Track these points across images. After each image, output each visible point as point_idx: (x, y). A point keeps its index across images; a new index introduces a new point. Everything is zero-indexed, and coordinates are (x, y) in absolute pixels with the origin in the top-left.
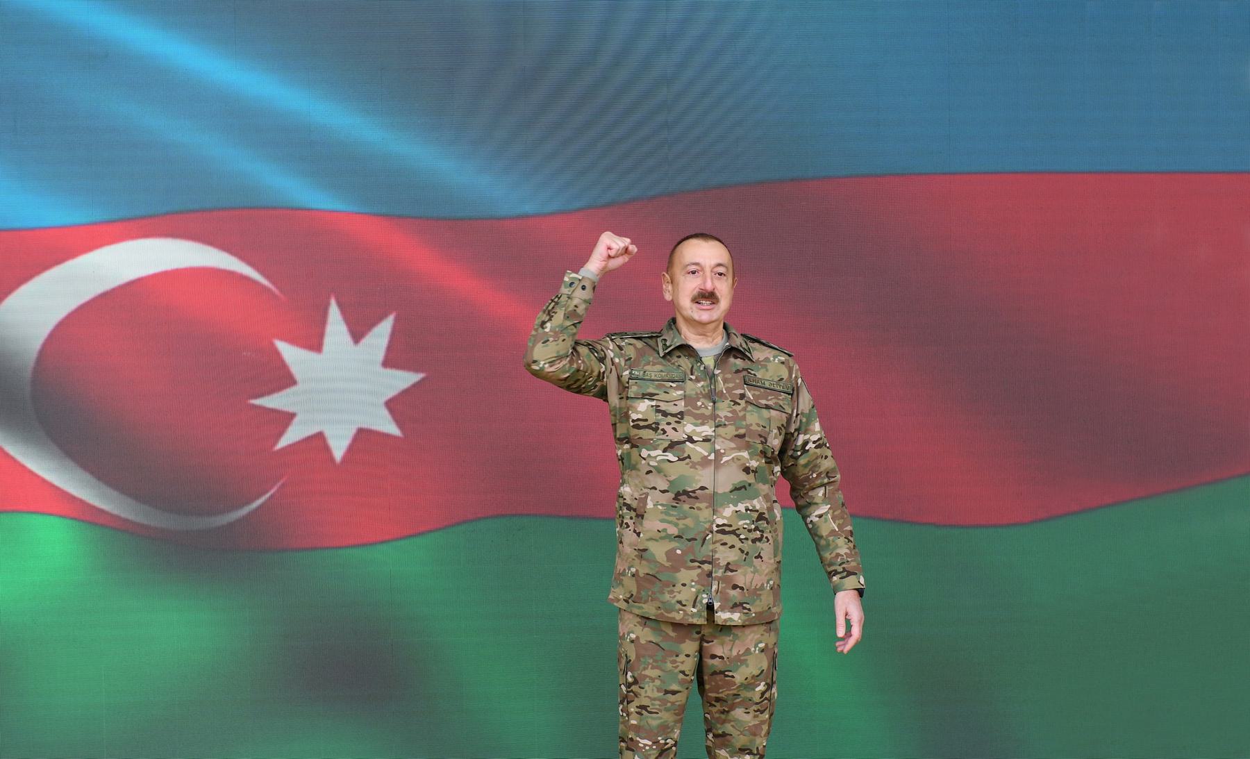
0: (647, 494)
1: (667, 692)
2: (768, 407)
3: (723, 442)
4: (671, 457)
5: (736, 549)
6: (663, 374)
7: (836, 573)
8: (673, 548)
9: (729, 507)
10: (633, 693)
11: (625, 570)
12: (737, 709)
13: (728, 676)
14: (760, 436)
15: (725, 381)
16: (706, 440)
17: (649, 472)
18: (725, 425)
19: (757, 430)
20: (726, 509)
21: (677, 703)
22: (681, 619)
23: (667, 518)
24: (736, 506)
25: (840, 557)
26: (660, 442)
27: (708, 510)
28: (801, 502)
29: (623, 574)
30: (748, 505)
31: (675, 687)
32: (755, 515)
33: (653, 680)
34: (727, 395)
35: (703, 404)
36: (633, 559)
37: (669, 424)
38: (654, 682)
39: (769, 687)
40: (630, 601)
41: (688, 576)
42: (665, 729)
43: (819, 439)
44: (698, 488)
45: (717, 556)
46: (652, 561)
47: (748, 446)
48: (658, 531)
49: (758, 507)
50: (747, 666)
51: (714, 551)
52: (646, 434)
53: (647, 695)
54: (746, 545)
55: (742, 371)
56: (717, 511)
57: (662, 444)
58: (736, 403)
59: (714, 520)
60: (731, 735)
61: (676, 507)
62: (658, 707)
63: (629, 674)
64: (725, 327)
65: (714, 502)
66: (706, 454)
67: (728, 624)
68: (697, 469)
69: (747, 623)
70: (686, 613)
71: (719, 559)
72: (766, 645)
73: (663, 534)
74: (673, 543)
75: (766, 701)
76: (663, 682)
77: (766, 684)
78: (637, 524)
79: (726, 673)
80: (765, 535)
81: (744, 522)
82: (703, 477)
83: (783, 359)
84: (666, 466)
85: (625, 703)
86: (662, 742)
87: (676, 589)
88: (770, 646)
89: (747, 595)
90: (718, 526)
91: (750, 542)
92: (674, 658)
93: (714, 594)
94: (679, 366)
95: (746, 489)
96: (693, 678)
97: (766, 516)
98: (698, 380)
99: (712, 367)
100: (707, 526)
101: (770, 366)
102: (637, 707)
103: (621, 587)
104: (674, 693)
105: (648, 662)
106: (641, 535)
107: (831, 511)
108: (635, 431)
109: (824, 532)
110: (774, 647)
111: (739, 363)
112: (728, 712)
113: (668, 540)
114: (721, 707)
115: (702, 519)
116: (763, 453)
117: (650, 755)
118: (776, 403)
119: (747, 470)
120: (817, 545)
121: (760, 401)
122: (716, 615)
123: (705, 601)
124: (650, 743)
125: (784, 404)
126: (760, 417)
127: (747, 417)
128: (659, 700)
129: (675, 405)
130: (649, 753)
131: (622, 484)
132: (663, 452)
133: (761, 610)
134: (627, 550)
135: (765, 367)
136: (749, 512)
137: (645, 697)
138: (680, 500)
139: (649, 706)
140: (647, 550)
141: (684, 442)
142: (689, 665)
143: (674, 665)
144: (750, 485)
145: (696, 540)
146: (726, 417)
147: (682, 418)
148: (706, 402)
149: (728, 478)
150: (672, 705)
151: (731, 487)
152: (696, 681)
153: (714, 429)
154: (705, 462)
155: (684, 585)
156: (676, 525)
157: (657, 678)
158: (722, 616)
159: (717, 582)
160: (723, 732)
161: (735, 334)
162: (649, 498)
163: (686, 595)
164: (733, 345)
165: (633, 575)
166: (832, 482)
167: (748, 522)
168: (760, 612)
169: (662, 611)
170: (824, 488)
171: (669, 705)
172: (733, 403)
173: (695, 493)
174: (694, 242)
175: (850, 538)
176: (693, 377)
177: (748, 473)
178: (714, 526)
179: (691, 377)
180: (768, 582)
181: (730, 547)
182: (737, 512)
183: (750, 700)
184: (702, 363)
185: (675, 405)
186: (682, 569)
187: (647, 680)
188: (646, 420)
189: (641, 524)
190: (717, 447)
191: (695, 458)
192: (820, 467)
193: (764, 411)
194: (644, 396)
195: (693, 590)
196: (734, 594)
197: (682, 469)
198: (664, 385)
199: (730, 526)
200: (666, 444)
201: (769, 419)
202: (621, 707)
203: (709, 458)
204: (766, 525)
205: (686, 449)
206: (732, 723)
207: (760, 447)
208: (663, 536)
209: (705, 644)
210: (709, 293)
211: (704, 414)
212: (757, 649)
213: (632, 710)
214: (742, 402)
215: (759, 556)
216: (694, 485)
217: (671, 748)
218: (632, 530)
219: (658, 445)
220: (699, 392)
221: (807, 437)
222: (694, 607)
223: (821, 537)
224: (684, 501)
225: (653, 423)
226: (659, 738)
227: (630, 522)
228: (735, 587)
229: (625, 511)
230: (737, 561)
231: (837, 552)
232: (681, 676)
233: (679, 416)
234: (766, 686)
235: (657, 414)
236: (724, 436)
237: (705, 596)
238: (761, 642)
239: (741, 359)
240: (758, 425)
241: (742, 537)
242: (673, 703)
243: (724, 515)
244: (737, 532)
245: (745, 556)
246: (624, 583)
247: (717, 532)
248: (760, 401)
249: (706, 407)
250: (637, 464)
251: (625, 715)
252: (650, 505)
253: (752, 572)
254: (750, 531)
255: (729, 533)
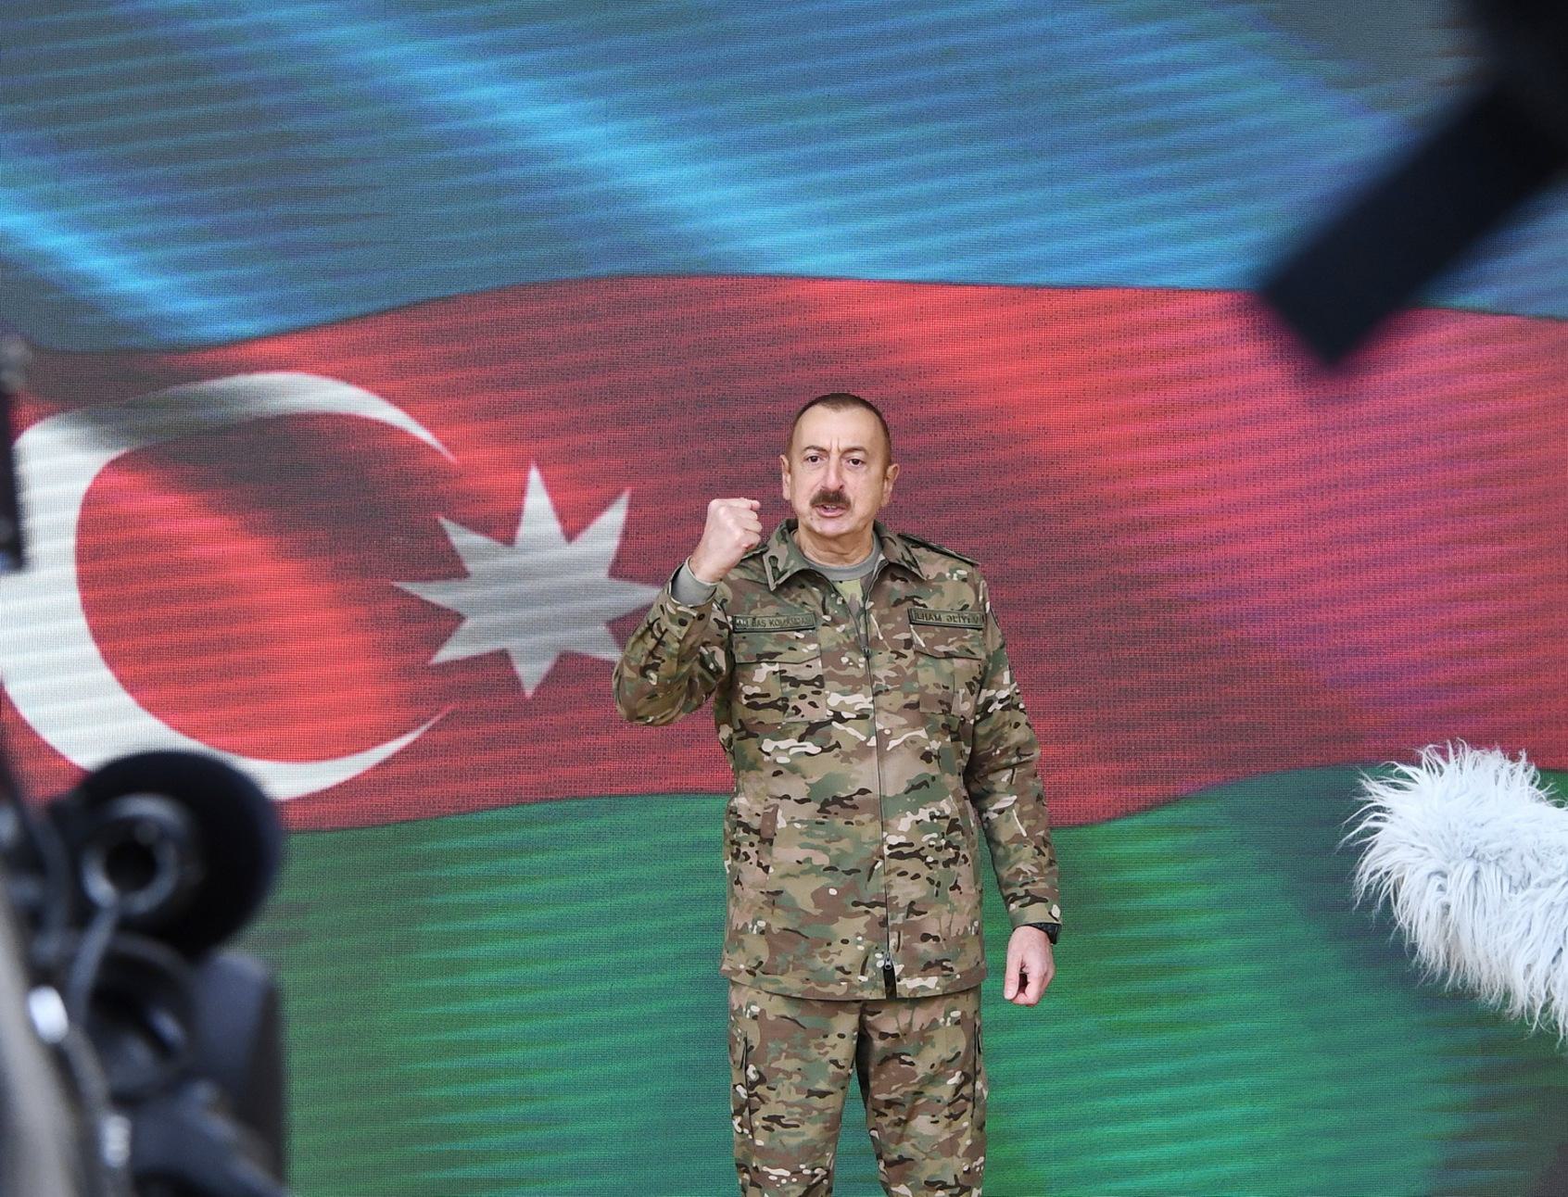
0: (776, 808)
1: (811, 1093)
2: (949, 656)
3: (886, 717)
4: (810, 747)
5: (923, 878)
6: (782, 619)
7: (1015, 898)
8: (823, 887)
9: (906, 816)
10: (759, 1097)
11: (746, 924)
12: (919, 1116)
13: (904, 1062)
14: (941, 702)
15: (881, 621)
16: (862, 716)
17: (777, 774)
18: (887, 690)
19: (937, 695)
20: (903, 820)
21: (829, 1112)
22: (845, 994)
23: (810, 841)
24: (915, 813)
25: (1022, 875)
26: (793, 726)
27: (873, 824)
28: (974, 788)
29: (744, 929)
30: (933, 809)
31: (822, 1086)
32: (945, 824)
33: (789, 1075)
34: (885, 643)
35: (850, 660)
36: (761, 908)
37: (803, 697)
38: (791, 1078)
39: (968, 1078)
40: (757, 971)
41: (853, 927)
42: (810, 1152)
43: (1008, 697)
44: (856, 791)
45: (893, 893)
46: (792, 908)
47: (924, 721)
48: (798, 862)
49: (948, 812)
50: (933, 1046)
51: (888, 886)
52: (769, 716)
53: (780, 1099)
54: (935, 872)
55: (904, 601)
56: (888, 825)
57: (795, 729)
58: (901, 656)
59: (884, 840)
60: (912, 1160)
61: (822, 823)
62: (797, 1116)
63: (752, 1068)
64: (876, 529)
65: (882, 810)
66: (863, 738)
67: (918, 996)
68: (851, 763)
69: (950, 990)
70: (851, 985)
71: (897, 897)
72: (963, 1013)
73: (806, 866)
74: (822, 878)
75: (962, 1101)
76: (805, 1077)
77: (963, 1073)
78: (763, 854)
79: (903, 1057)
80: (962, 853)
81: (929, 836)
82: (863, 775)
83: (963, 573)
84: (804, 762)
85: (746, 1113)
86: (807, 1172)
87: (831, 949)
88: (970, 1015)
89: (945, 948)
90: (890, 847)
91: (941, 867)
92: (822, 1040)
93: (892, 951)
94: (804, 603)
95: (928, 786)
96: (850, 1071)
97: (959, 823)
98: (835, 622)
99: (859, 598)
100: (874, 848)
101: (946, 587)
102: (764, 1119)
103: (740, 951)
104: (822, 1094)
105: (781, 1049)
106: (771, 870)
107: (1017, 805)
108: (754, 713)
109: (1004, 836)
110: (974, 1017)
111: (898, 586)
112: (906, 1122)
113: (814, 875)
114: (895, 1115)
115: (865, 839)
116: (946, 727)
117: (788, 1192)
118: (961, 647)
119: (927, 757)
120: (993, 855)
121: (936, 648)
122: (898, 983)
123: (880, 964)
124: (787, 1173)
125: (973, 646)
126: (939, 672)
127: (920, 674)
128: (800, 1106)
129: (808, 666)
130: (786, 1189)
131: (736, 795)
132: (799, 741)
133: (968, 968)
134: (750, 893)
135: (939, 590)
136: (935, 820)
137: (777, 1102)
138: (829, 812)
139: (783, 1117)
140: (782, 892)
141: (829, 723)
142: (842, 1049)
143: (821, 1051)
144: (933, 778)
145: (859, 871)
146: (887, 678)
147: (822, 686)
148: (853, 655)
149: (897, 773)
150: (820, 1114)
151: (905, 786)
152: (855, 1076)
153: (871, 698)
154: (862, 751)
155: (845, 942)
156: (826, 851)
157: (795, 1073)
158: (908, 985)
159: (896, 934)
160: (900, 1156)
161: (890, 539)
162: (780, 812)
163: (848, 956)
164: (892, 560)
165: (762, 932)
166: (1024, 762)
167: (935, 835)
168: (967, 971)
169: (813, 984)
170: (1011, 771)
171: (815, 1113)
172: (895, 656)
173: (852, 799)
174: (818, 410)
175: (1042, 848)
176: (828, 618)
177: (929, 761)
178: (885, 847)
179: (825, 617)
180: (972, 924)
181: (913, 878)
182: (918, 822)
183: (939, 1101)
184: (838, 594)
185: (808, 666)
186: (840, 918)
187: (781, 1075)
188: (768, 695)
189: (770, 853)
190: (879, 726)
191: (846, 747)
192: (1006, 740)
193: (944, 663)
194: (761, 658)
195: (861, 948)
196: (926, 948)
197: (830, 763)
198: (786, 636)
199: (911, 845)
200: (802, 729)
201: (952, 674)
202: (738, 1119)
203: (868, 744)
204: (961, 838)
205: (833, 734)
206: (913, 1141)
207: (942, 719)
208: (805, 868)
209: (869, 1018)
210: (834, 493)
211: (854, 676)
212: (949, 1019)
213: (757, 1123)
214: (909, 653)
215: (956, 887)
216: (849, 787)
217: (822, 1180)
218: (755, 863)
219: (790, 731)
220: (842, 642)
221: (992, 692)
222: (862, 974)
223: (998, 844)
224: (836, 814)
225: (779, 700)
226: (802, 1166)
227: (751, 851)
228: (925, 937)
229: (741, 834)
230: (924, 897)
231: (1018, 867)
232: (832, 1068)
233: (817, 683)
234: (963, 1078)
235: (783, 685)
236: (888, 707)
237: (879, 955)
238: (954, 1009)
239: (902, 579)
240: (937, 686)
241: (930, 859)
242: (821, 1111)
243: (900, 829)
244: (921, 852)
245: (936, 888)
246: (745, 944)
247: (891, 856)
248: (936, 648)
249: (854, 663)
250: (756, 761)
251: (746, 1131)
252: (782, 823)
253: (949, 912)
254: (939, 849)
255: (910, 856)
